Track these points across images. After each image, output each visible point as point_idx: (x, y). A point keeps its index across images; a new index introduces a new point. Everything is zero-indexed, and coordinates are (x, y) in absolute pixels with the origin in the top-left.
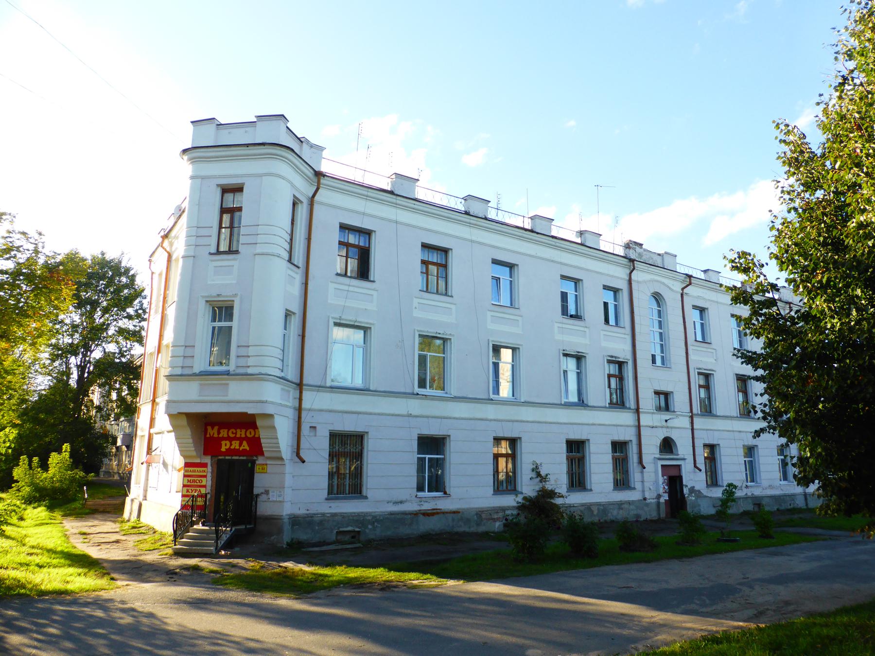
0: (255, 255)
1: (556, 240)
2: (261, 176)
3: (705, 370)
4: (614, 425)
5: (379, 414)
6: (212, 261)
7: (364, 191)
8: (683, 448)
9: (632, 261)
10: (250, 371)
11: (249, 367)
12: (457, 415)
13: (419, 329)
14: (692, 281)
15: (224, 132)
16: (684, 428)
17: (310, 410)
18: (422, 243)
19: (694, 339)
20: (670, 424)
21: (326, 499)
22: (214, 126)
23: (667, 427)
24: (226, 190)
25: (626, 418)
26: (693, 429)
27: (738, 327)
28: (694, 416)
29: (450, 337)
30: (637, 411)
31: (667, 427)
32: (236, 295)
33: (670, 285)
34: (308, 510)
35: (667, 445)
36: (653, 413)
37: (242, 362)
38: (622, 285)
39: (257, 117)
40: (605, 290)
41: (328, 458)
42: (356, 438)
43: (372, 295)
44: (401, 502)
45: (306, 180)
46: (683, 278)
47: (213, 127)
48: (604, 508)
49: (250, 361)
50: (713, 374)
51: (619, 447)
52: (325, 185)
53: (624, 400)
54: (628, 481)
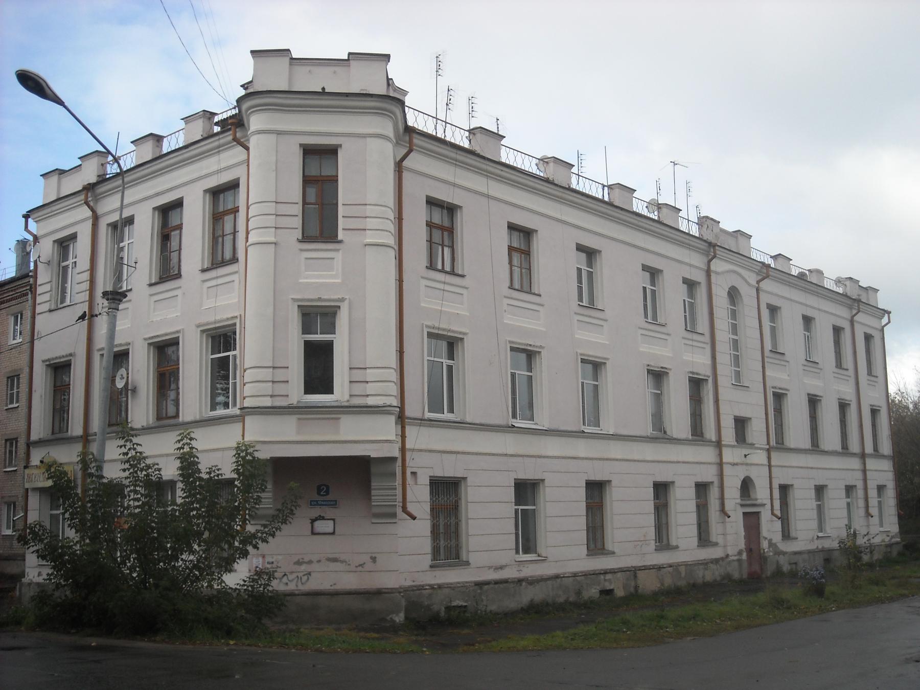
0: (366, 245)
1: (639, 219)
2: (365, 137)
3: (780, 389)
4: (697, 463)
5: (477, 454)
6: (301, 250)
7: (452, 154)
8: (761, 493)
9: (711, 245)
10: (371, 401)
11: (367, 396)
12: (550, 454)
13: (429, 323)
14: (718, 252)
15: (301, 70)
16: (762, 465)
17: (413, 450)
18: (427, 197)
19: (508, 284)
20: (750, 460)
21: (431, 567)
22: (287, 60)
23: (747, 464)
24: (309, 152)
25: (707, 454)
26: (770, 466)
27: (731, 305)
28: (771, 449)
29: (540, 350)
30: (719, 444)
31: (747, 464)
32: (342, 300)
33: (745, 276)
34: (414, 581)
35: (746, 486)
36: (733, 446)
37: (358, 389)
38: (699, 277)
39: (350, 54)
40: (644, 272)
41: (429, 512)
42: (452, 485)
43: (462, 294)
44: (502, 568)
45: (840, 304)
46: (759, 268)
47: (286, 60)
48: (690, 566)
49: (370, 388)
50: (787, 394)
51: (702, 488)
52: (699, 249)
53: (703, 431)
54: (458, 548)
